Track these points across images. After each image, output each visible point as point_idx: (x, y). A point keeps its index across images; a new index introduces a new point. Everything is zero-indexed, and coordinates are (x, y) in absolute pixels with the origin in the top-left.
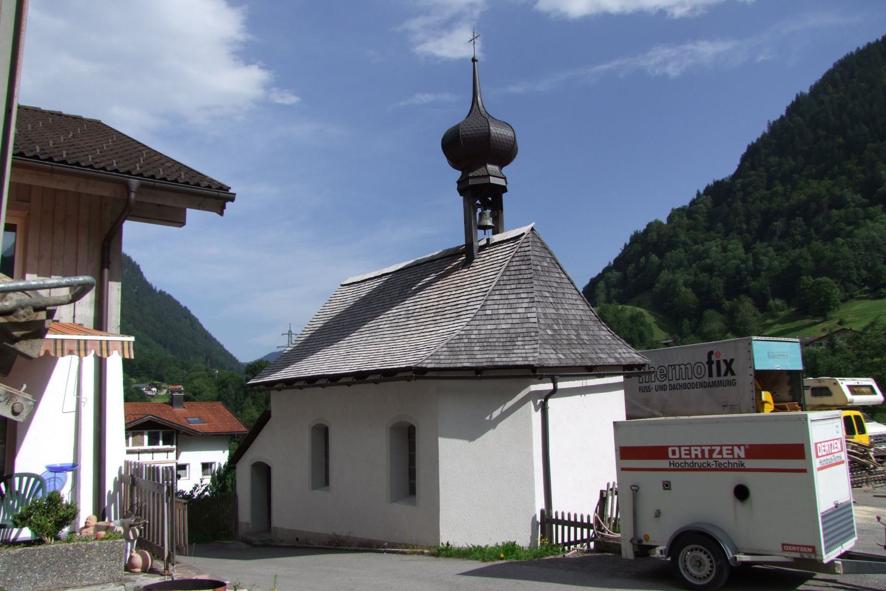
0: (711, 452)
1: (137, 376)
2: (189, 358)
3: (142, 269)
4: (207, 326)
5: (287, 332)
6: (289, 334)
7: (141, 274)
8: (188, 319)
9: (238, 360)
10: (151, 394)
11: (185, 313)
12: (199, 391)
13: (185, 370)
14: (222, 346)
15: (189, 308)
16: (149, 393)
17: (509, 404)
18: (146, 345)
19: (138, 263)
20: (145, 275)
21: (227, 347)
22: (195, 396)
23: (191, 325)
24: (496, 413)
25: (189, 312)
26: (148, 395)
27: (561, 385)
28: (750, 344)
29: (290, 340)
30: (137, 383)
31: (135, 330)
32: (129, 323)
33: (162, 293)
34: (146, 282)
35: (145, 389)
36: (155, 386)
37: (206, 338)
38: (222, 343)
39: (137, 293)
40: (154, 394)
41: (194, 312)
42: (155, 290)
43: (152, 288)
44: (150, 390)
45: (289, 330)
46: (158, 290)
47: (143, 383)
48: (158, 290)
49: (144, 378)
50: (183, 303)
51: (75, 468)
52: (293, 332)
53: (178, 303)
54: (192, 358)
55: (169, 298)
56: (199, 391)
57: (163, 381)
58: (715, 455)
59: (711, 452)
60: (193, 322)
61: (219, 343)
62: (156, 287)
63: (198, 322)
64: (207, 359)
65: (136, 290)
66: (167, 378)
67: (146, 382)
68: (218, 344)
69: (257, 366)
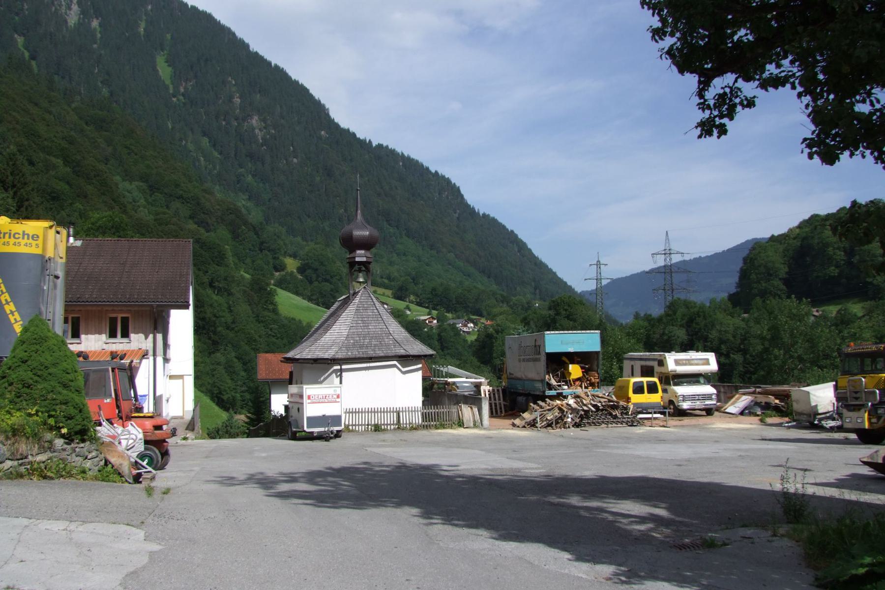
0: (326, 397)
1: (455, 311)
2: (516, 289)
3: (463, 191)
4: (536, 252)
5: (595, 262)
6: (597, 265)
7: (462, 196)
8: (515, 245)
9: (574, 289)
10: (468, 330)
11: (512, 238)
12: (502, 329)
13: (505, 303)
14: (555, 274)
15: (516, 232)
16: (465, 329)
17: (327, 374)
18: (469, 276)
19: (457, 185)
20: (466, 197)
21: (560, 275)
22: (498, 334)
23: (519, 251)
24: (322, 378)
25: (516, 236)
26: (463, 331)
27: (344, 367)
28: (544, 336)
29: (599, 271)
30: (453, 319)
31: (457, 260)
32: (449, 252)
33: (485, 216)
34: (468, 206)
35: (460, 325)
36: (472, 321)
37: (536, 264)
38: (554, 270)
39: (458, 218)
40: (471, 330)
41: (522, 235)
42: (478, 213)
43: (475, 211)
44: (466, 326)
45: (597, 260)
46: (481, 213)
47: (459, 318)
48: (481, 213)
49: (460, 313)
50: (510, 227)
51: (149, 395)
52: (602, 262)
53: (504, 227)
54: (518, 288)
55: (494, 221)
56: (502, 329)
57: (481, 315)
58: (327, 398)
59: (326, 397)
60: (521, 246)
61: (551, 270)
62: (478, 210)
63: (527, 247)
64: (535, 289)
65: (457, 215)
66: (485, 313)
67: (463, 317)
68: (550, 271)
69: (559, 301)
